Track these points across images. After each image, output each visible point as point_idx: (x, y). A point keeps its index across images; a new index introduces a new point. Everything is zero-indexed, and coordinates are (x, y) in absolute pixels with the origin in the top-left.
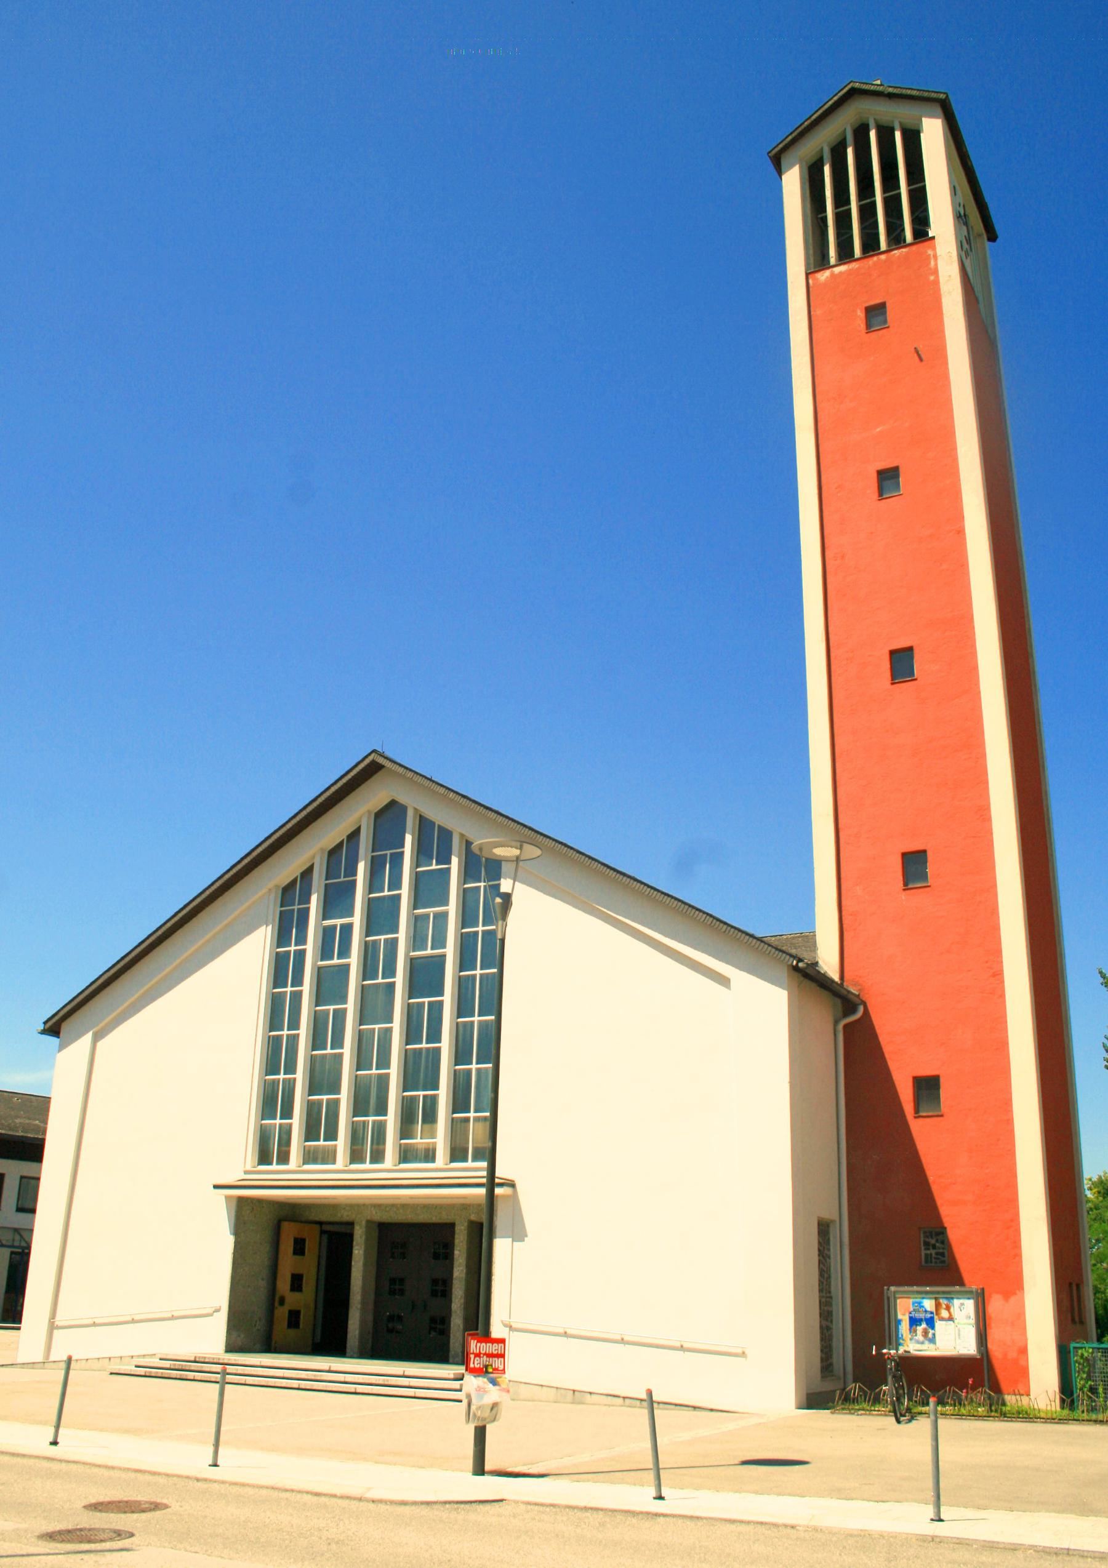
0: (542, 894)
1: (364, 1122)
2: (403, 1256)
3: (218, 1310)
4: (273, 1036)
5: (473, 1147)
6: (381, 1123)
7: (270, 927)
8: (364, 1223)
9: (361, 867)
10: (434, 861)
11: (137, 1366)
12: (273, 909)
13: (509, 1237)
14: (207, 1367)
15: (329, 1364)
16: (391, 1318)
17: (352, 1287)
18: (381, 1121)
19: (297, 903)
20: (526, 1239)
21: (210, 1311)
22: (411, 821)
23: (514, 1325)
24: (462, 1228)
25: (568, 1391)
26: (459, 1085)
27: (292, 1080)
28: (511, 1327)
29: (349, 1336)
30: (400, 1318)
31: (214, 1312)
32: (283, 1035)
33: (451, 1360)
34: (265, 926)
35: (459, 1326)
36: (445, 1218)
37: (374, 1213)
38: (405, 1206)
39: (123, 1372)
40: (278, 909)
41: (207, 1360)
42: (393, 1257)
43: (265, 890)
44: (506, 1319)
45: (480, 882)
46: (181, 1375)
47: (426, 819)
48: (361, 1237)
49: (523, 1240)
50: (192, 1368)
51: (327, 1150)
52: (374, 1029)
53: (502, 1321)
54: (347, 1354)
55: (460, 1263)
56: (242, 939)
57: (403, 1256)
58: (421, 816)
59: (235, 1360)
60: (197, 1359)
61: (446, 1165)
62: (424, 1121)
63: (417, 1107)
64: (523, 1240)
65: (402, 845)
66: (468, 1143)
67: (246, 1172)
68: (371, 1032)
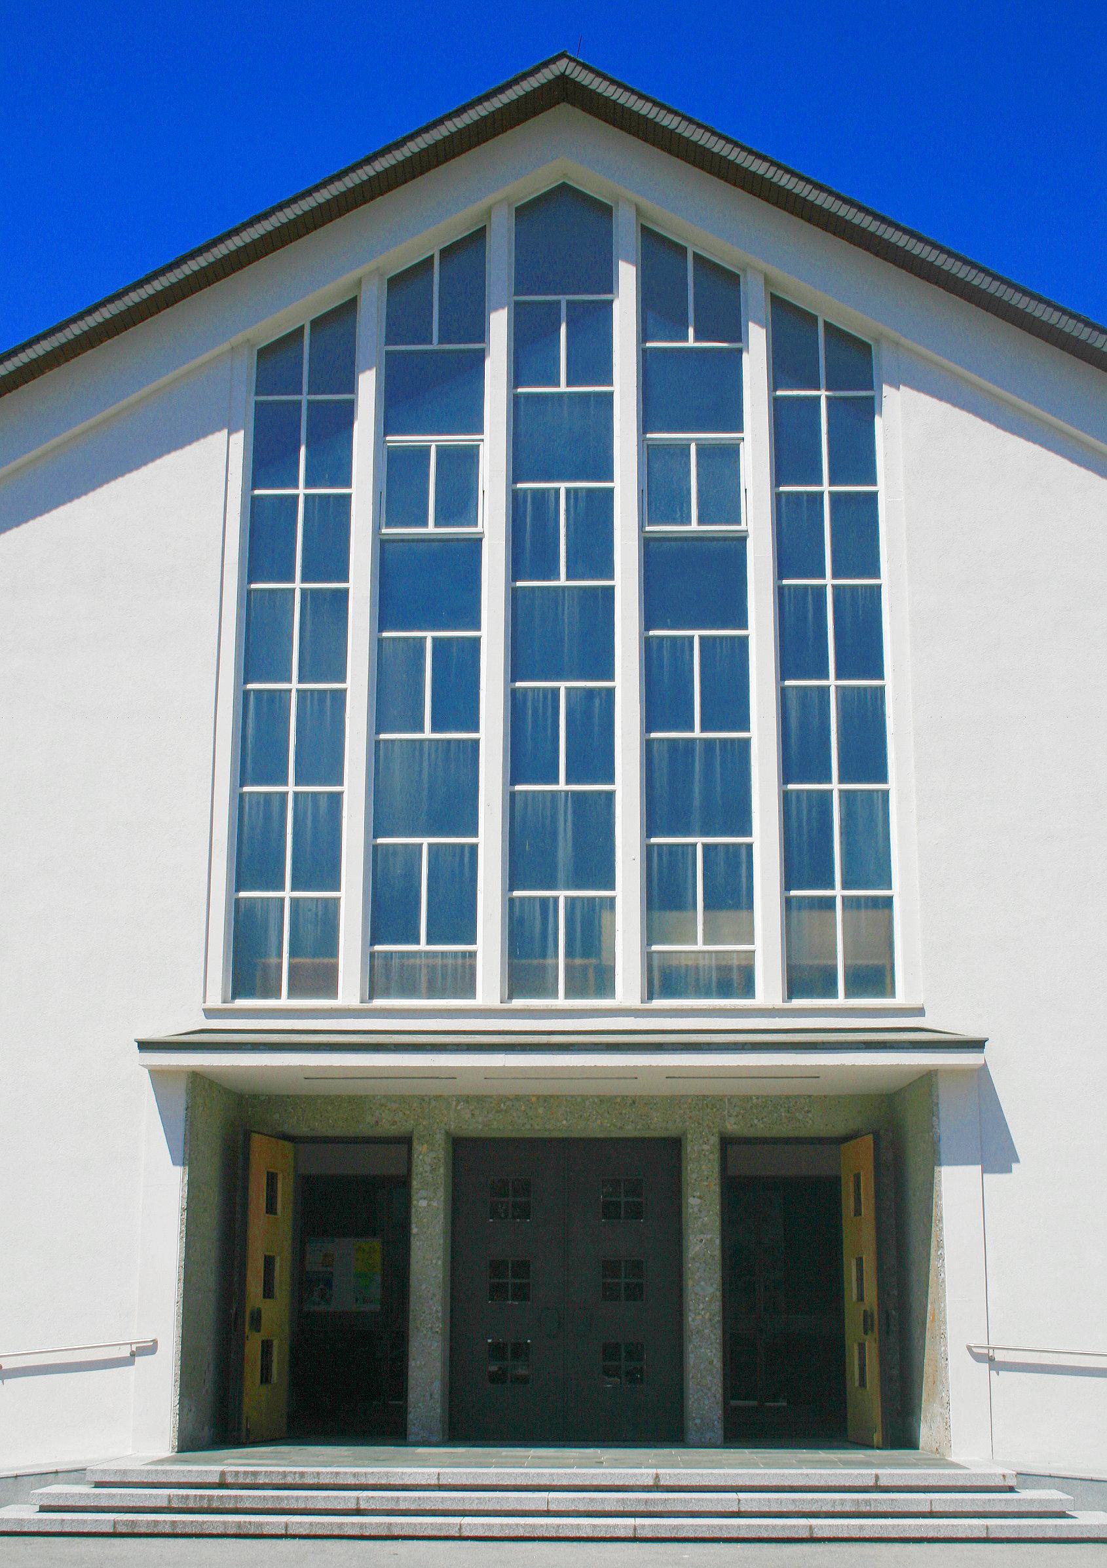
0: (992, 428)
1: (544, 901)
2: (524, 1211)
3: (150, 1349)
4: (258, 692)
5: (846, 968)
6: (326, 908)
7: (239, 438)
8: (439, 1138)
9: (499, 324)
10: (691, 331)
11: (44, 1509)
12: (246, 400)
13: (978, 1164)
14: (490, 1500)
15: (220, 1468)
16: (498, 1351)
17: (413, 1282)
18: (326, 900)
19: (305, 388)
20: (1014, 1166)
21: (125, 1352)
22: (625, 232)
23: (999, 1356)
24: (706, 1147)
25: (8, 1480)
26: (800, 826)
27: (323, 804)
28: (991, 1360)
29: (414, 1395)
30: (520, 1351)
31: (133, 1354)
32: (290, 691)
33: (692, 1436)
34: (225, 432)
35: (711, 1363)
36: (658, 1126)
37: (468, 1116)
38: (576, 1103)
39: (893, 1535)
40: (253, 399)
41: (261, 1480)
42: (494, 1214)
43: (225, 346)
44: (978, 1340)
45: (818, 389)
46: (239, 1524)
47: (485, 236)
48: (433, 1170)
49: (1009, 1171)
50: (403, 1506)
51: (683, 971)
52: (556, 691)
53: (969, 1348)
54: (411, 1438)
55: (704, 1225)
56: (875, 460)
57: (524, 1211)
58: (483, 229)
59: (355, 1475)
60: (230, 1480)
61: (224, 1002)
62: (706, 907)
63: (690, 880)
64: (1009, 1171)
65: (608, 284)
66: (835, 958)
67: (210, 1013)
68: (545, 697)
